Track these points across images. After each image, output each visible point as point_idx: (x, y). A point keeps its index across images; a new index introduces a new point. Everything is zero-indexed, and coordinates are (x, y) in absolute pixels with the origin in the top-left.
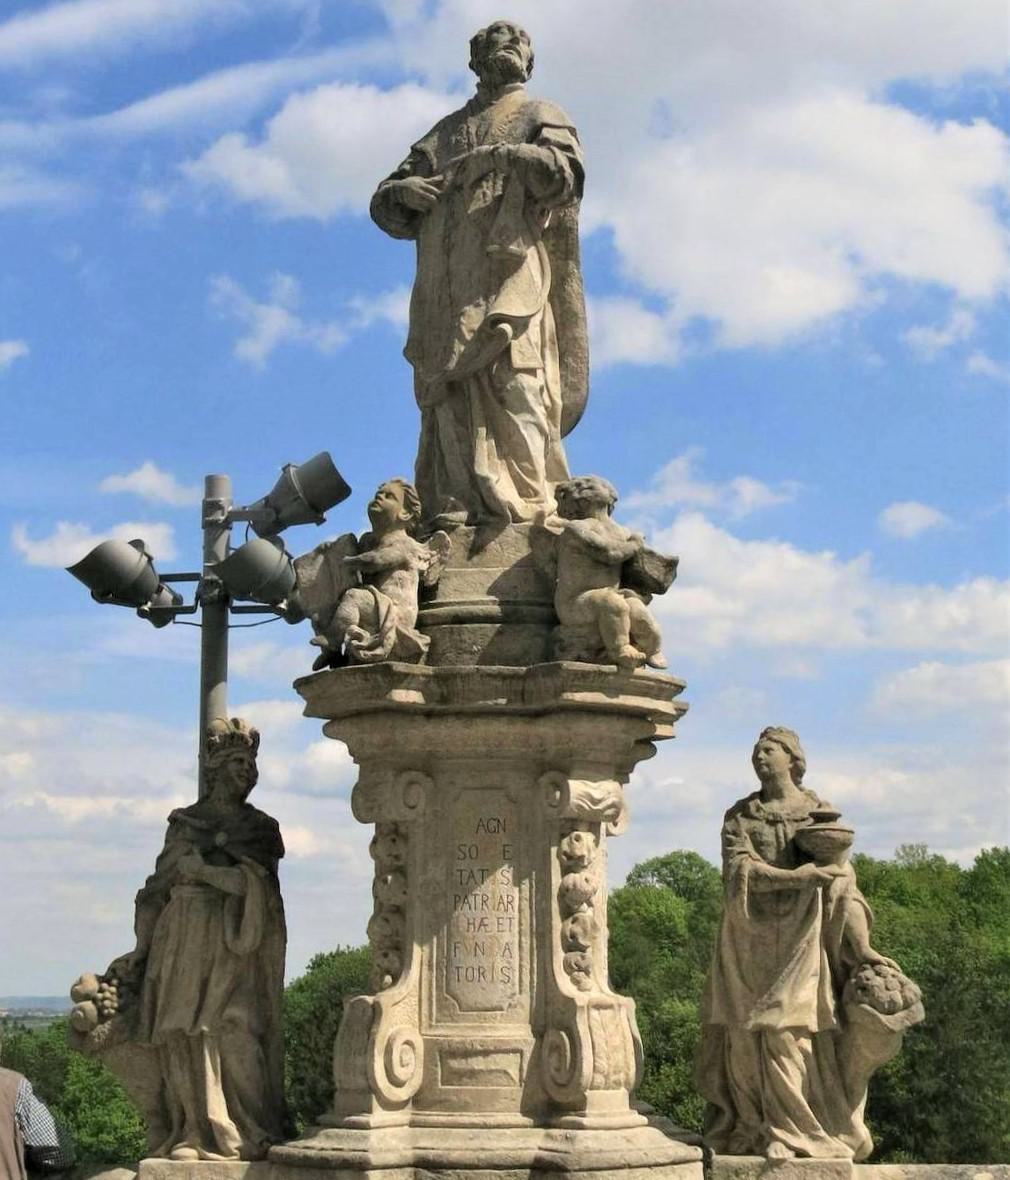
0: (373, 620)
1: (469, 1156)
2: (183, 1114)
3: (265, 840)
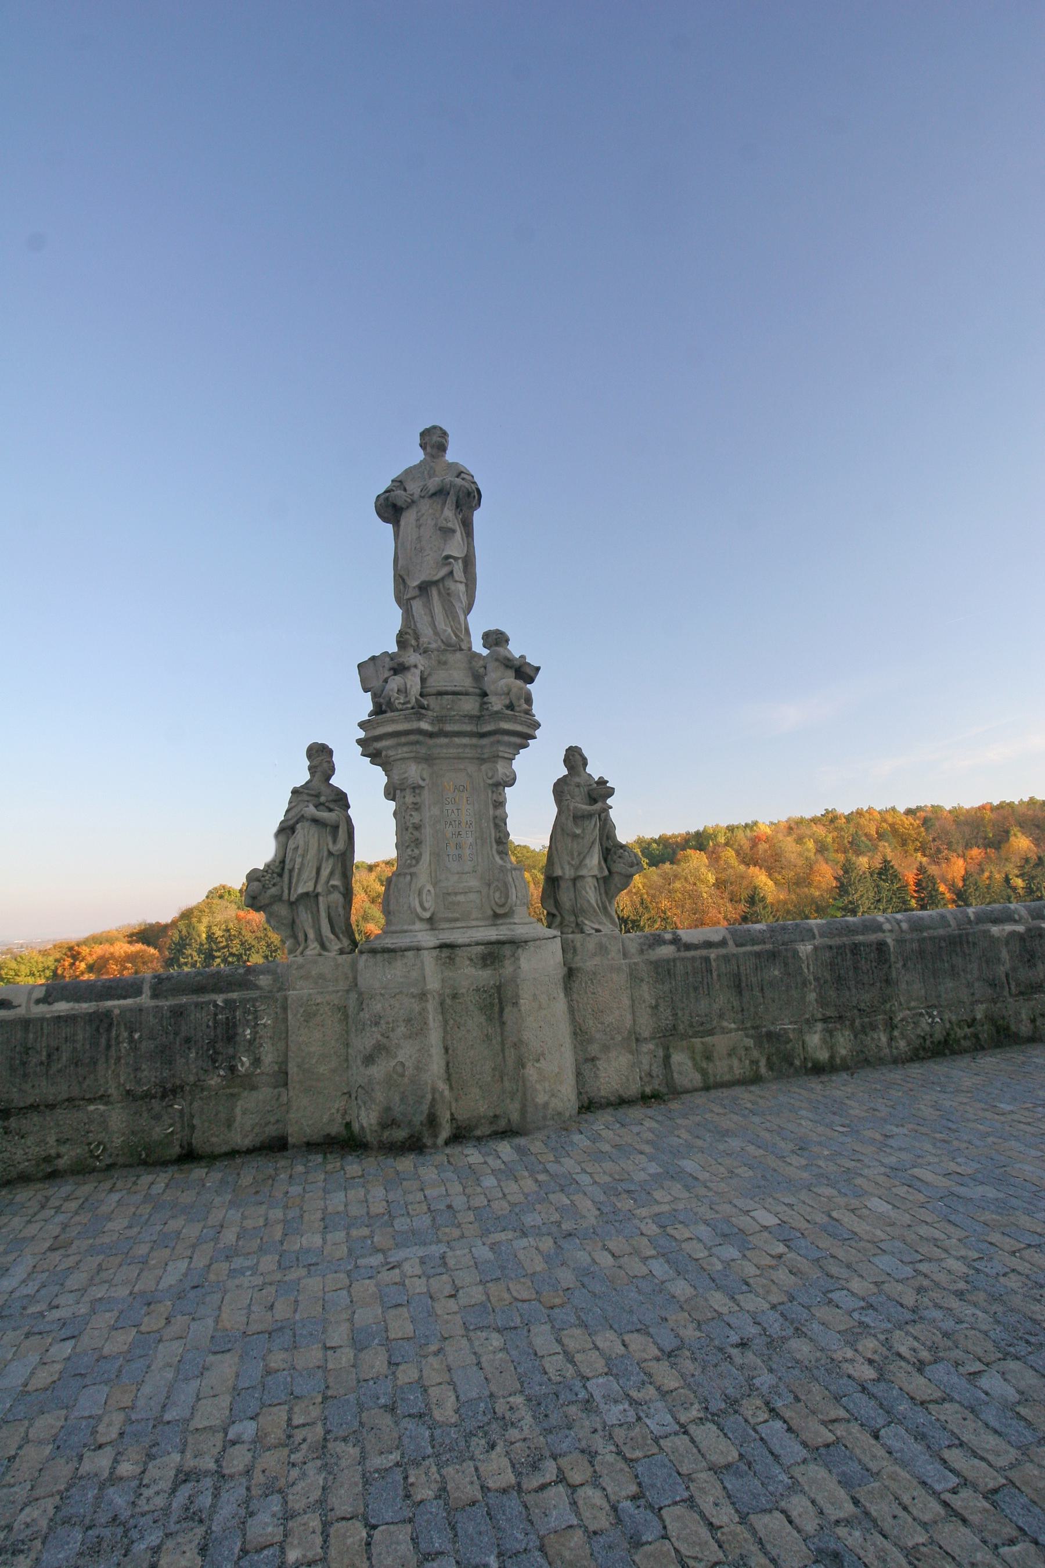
0: (403, 691)
1: (467, 941)
2: (306, 936)
3: (341, 800)
